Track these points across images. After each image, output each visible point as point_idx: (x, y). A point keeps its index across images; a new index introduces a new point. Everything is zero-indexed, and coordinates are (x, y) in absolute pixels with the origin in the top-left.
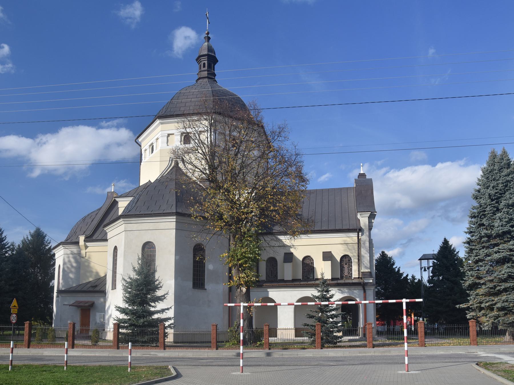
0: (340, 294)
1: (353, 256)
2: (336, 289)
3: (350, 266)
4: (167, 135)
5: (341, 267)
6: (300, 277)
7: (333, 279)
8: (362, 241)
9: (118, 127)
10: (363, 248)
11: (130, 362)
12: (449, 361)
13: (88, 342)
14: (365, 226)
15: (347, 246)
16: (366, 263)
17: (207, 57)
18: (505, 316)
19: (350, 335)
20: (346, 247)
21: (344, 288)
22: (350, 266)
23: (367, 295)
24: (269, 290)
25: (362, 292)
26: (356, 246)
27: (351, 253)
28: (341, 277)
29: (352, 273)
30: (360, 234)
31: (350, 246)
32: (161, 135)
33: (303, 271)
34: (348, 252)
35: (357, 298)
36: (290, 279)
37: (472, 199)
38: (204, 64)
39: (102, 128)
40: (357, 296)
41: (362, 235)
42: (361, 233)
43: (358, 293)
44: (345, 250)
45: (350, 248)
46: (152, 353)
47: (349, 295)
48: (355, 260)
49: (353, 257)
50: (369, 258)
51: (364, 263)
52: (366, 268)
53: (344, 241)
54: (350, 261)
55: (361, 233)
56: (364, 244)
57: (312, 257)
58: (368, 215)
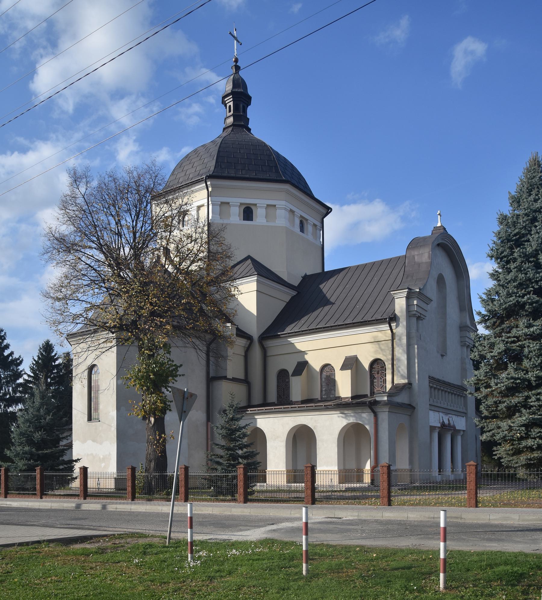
0: (344, 420)
1: (386, 357)
2: (338, 412)
3: (383, 375)
4: (220, 203)
5: (371, 378)
6: (318, 396)
7: (353, 398)
8: (398, 336)
9: (371, 200)
10: (398, 346)
11: (445, 529)
12: (231, 534)
13: (229, 497)
14: (401, 311)
15: (379, 345)
16: (402, 370)
17: (231, 96)
18: (513, 455)
19: (463, 490)
20: (377, 346)
21: (348, 410)
22: (383, 375)
23: (380, 420)
24: (256, 417)
25: (372, 415)
26: (390, 343)
27: (383, 355)
28: (371, 393)
29: (386, 386)
30: (394, 325)
31: (382, 344)
32: (284, 207)
33: (278, 386)
34: (380, 353)
35: (367, 424)
36: (299, 399)
37: (486, 255)
38: (230, 106)
39: (349, 203)
40: (366, 422)
41: (397, 326)
42: (395, 324)
43: (367, 418)
44: (376, 352)
45: (383, 347)
46: (516, 517)
47: (356, 420)
48: (388, 366)
49: (387, 361)
50: (406, 362)
51: (400, 369)
52: (402, 377)
53: (375, 337)
54: (383, 367)
55: (395, 324)
56: (400, 339)
57: (333, 365)
58: (405, 294)
